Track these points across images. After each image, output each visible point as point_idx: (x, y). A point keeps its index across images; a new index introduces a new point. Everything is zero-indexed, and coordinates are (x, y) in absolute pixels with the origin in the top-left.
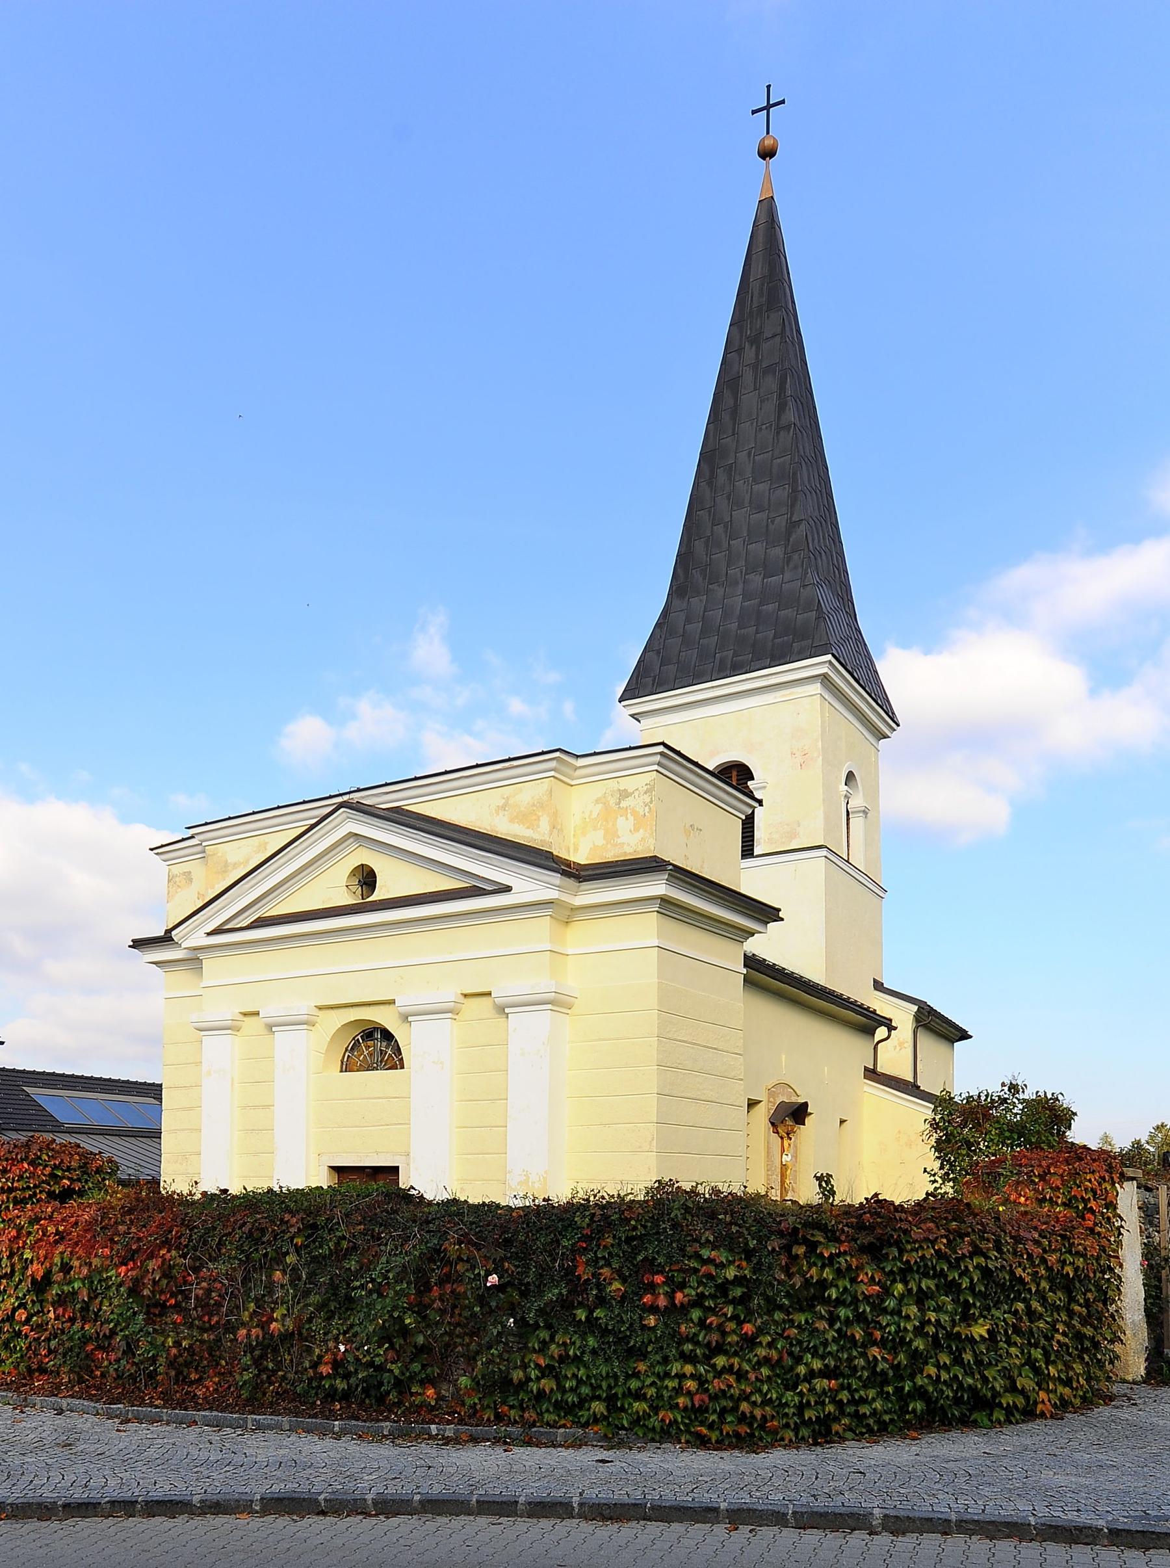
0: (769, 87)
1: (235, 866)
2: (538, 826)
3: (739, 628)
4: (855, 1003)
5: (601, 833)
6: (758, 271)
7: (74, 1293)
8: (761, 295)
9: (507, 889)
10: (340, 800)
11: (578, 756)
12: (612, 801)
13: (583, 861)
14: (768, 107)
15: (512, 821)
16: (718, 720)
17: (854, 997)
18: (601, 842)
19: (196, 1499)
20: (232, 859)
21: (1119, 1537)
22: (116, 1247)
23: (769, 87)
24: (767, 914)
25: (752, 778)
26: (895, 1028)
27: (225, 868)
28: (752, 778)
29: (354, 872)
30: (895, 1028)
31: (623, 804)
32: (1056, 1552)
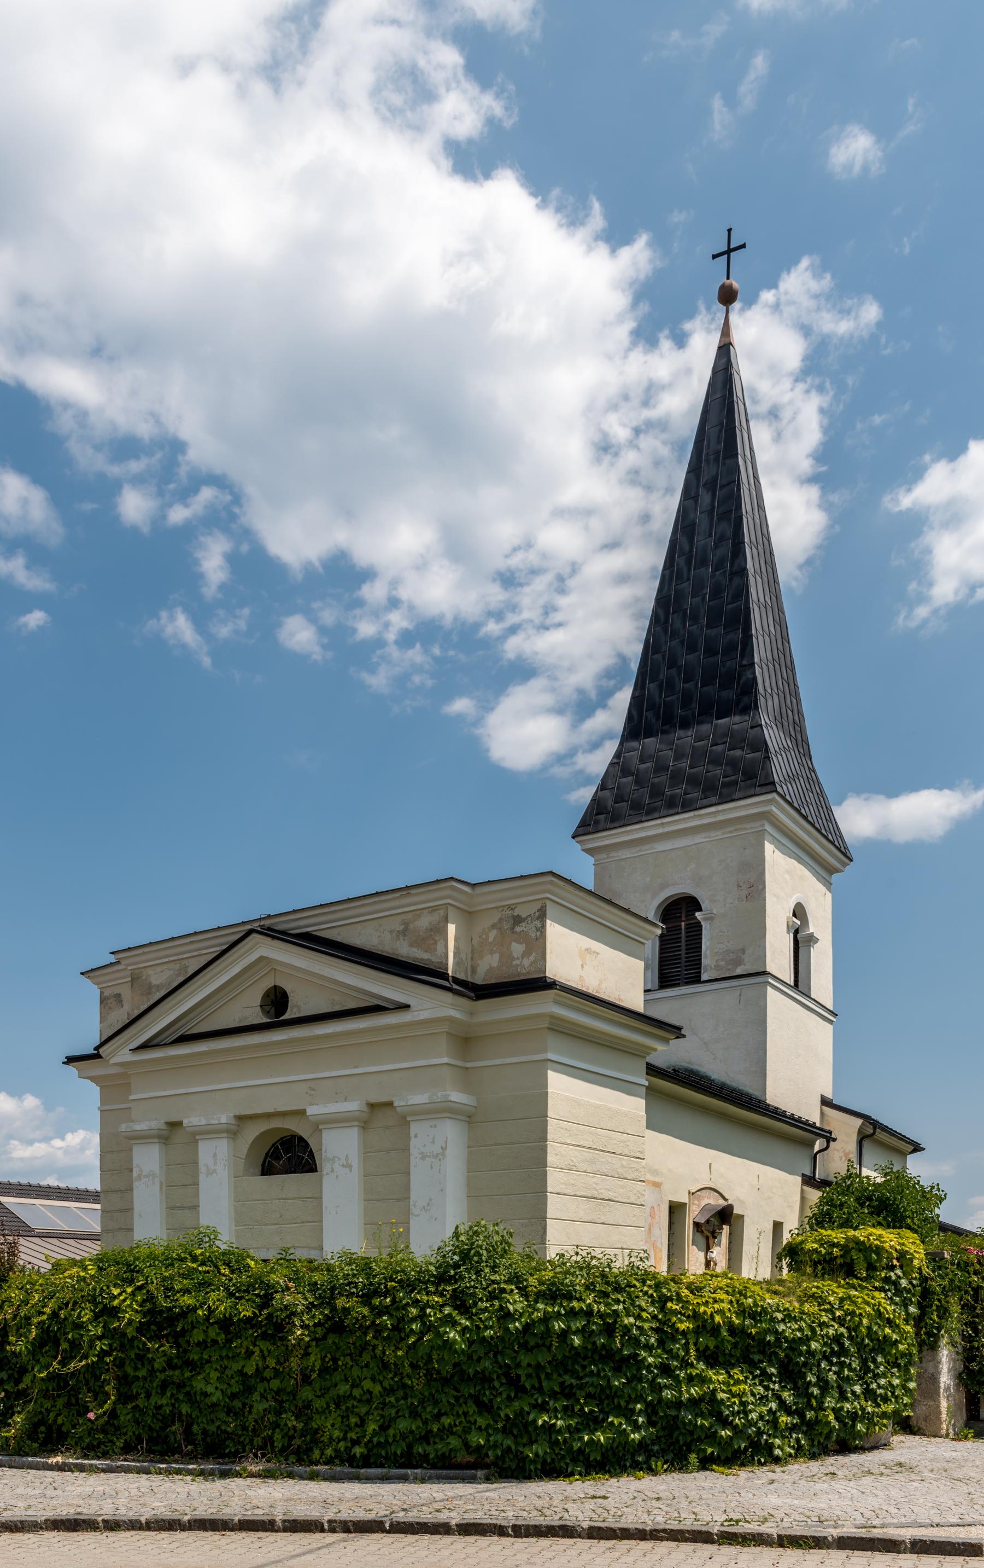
0: (729, 230)
1: (158, 987)
2: (436, 950)
3: (691, 767)
4: (799, 1120)
5: (497, 956)
6: (713, 419)
7: (163, 1394)
8: (719, 442)
9: (406, 1007)
10: (248, 927)
11: (474, 886)
12: (506, 926)
13: (480, 983)
14: (729, 252)
15: (411, 945)
16: (674, 852)
17: (798, 1114)
18: (495, 964)
19: (143, 1520)
20: (155, 980)
21: (845, 1543)
22: (213, 1359)
23: (729, 230)
24: (676, 1031)
25: (700, 909)
26: (834, 1140)
27: (150, 989)
28: (700, 909)
29: (266, 995)
30: (834, 1140)
31: (518, 929)
32: (791, 1556)
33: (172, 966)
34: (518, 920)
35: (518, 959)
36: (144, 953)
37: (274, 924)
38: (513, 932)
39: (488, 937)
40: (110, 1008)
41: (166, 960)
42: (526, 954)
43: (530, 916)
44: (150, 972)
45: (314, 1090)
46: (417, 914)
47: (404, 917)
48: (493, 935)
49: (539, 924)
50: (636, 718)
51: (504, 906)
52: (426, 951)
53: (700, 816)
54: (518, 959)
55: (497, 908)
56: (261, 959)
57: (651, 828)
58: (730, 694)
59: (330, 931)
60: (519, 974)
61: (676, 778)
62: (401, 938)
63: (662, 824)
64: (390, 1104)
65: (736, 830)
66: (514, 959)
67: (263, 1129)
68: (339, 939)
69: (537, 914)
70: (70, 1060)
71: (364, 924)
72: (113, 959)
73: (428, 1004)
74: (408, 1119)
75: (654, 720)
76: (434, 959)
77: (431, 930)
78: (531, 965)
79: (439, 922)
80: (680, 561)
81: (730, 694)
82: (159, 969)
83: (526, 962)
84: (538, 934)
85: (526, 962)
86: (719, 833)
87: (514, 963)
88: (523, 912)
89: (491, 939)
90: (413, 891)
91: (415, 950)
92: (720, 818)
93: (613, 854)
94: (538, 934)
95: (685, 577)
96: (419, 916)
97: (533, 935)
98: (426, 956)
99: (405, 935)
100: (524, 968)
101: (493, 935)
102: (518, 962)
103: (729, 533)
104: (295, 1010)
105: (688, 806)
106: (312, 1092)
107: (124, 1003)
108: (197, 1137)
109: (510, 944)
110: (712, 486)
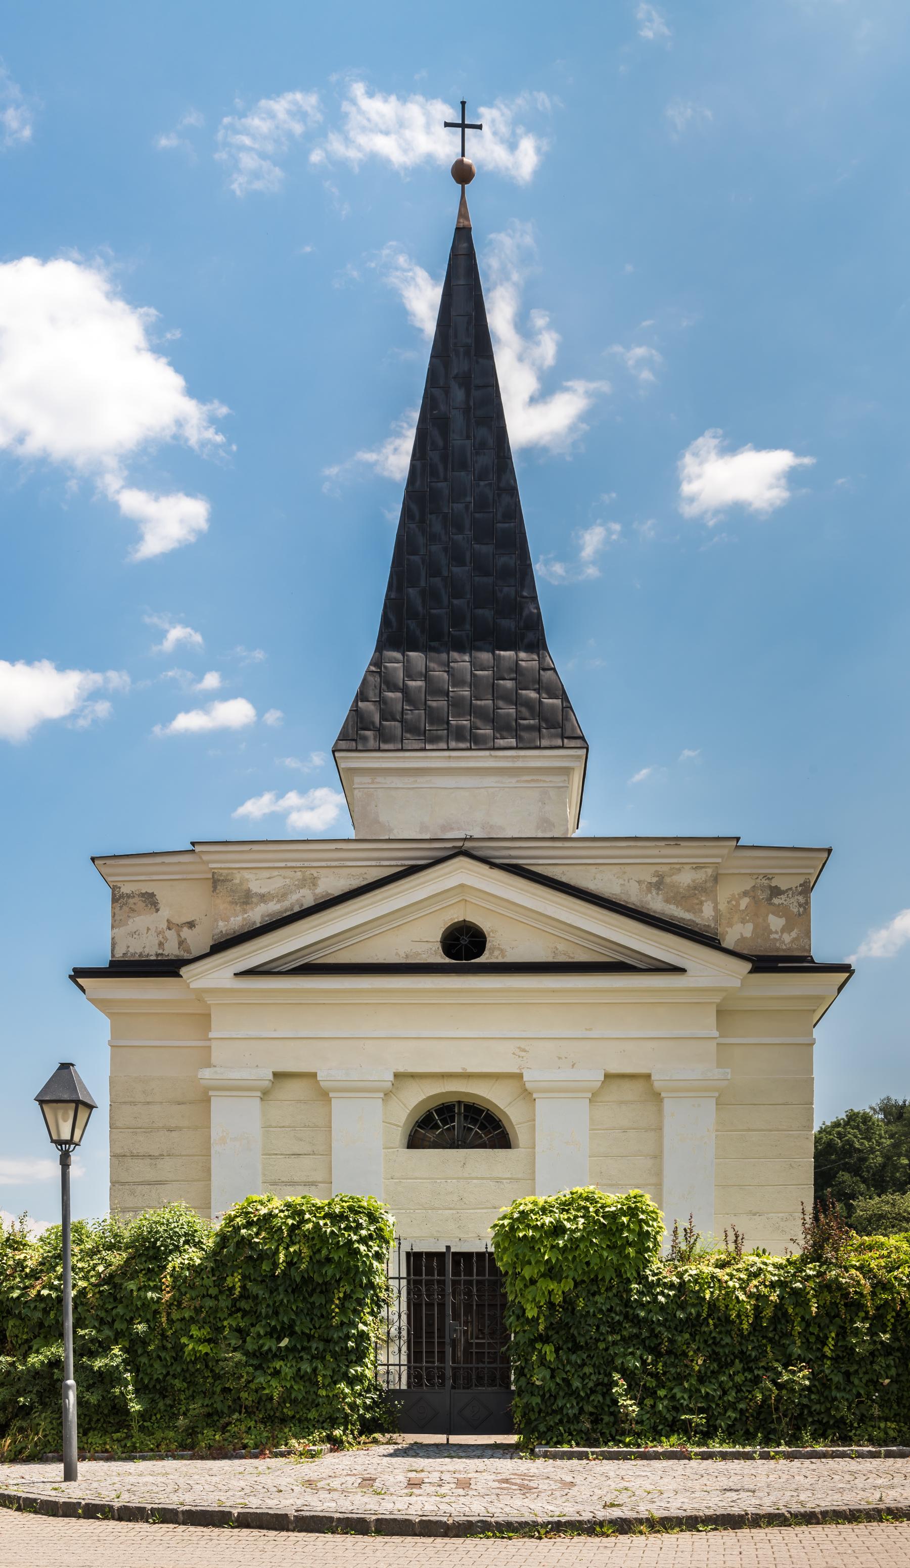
5: (750, 927)
12: (762, 896)
15: (667, 901)
20: (257, 884)
31: (776, 901)
33: (289, 873)
34: (776, 891)
35: (776, 932)
36: (250, 851)
37: (474, 848)
38: (771, 904)
39: (738, 904)
40: (133, 910)
41: (283, 864)
42: (786, 929)
43: (791, 889)
44: (247, 875)
45: (524, 1050)
46: (678, 868)
47: (658, 868)
48: (744, 902)
49: (801, 899)
50: (395, 624)
51: (759, 874)
52: (688, 911)
53: (496, 757)
54: (776, 932)
55: (750, 874)
56: (462, 886)
57: (435, 759)
58: (508, 624)
59: (550, 868)
60: (778, 949)
61: (457, 705)
62: (654, 892)
63: (450, 757)
64: (314, 1075)
65: (533, 780)
66: (771, 932)
67: (422, 1097)
68: (564, 879)
69: (800, 889)
70: (79, 973)
71: (601, 868)
72: (191, 848)
73: (708, 971)
74: (331, 1095)
75: (418, 632)
76: (698, 921)
77: (695, 888)
78: (792, 941)
79: (706, 882)
80: (434, 456)
81: (508, 624)
82: (266, 874)
83: (787, 938)
84: (801, 910)
85: (787, 938)
86: (514, 780)
87: (772, 936)
88: (783, 883)
89: (743, 907)
90: (683, 844)
91: (673, 907)
92: (519, 764)
93: (379, 779)
94: (801, 910)
95: (442, 475)
96: (679, 870)
97: (795, 910)
98: (688, 916)
99: (658, 889)
100: (785, 941)
101: (744, 902)
102: (777, 936)
103: (491, 442)
104: (496, 953)
105: (477, 742)
106: (523, 1054)
107: (161, 906)
108: (211, 1093)
109: (767, 916)
110: (465, 381)
